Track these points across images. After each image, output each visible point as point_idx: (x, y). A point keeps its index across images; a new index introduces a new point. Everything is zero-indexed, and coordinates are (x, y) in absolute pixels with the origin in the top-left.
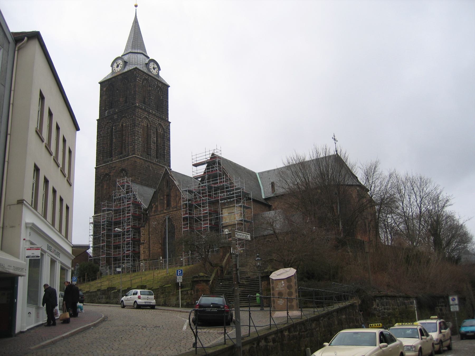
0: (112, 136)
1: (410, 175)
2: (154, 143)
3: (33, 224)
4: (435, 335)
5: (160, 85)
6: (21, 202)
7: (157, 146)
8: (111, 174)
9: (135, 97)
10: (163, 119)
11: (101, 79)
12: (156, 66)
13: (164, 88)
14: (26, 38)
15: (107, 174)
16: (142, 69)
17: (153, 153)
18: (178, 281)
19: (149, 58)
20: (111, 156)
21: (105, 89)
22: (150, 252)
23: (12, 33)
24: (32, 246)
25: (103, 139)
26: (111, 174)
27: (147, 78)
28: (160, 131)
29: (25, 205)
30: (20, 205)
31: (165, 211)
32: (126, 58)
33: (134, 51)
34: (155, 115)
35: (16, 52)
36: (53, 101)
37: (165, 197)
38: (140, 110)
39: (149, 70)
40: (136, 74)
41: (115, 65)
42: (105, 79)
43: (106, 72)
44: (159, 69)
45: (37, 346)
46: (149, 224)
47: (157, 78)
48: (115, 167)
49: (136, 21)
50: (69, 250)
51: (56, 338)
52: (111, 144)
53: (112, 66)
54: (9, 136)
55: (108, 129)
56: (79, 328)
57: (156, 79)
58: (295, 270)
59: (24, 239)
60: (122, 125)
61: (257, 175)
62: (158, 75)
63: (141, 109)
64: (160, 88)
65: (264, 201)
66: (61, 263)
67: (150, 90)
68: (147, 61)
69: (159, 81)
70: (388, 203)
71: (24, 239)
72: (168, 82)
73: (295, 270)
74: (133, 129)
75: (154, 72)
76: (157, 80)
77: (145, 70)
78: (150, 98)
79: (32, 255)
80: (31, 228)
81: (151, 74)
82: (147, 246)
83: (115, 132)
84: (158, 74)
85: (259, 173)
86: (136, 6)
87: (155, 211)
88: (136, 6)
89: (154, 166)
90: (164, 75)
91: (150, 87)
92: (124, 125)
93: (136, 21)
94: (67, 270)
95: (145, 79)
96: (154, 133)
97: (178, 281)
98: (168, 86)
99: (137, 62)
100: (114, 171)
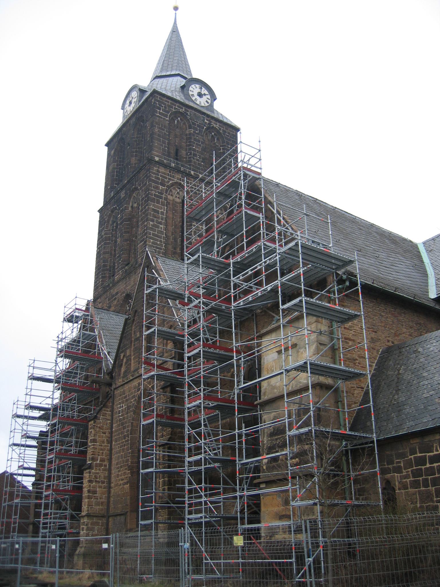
4: (155, 168)
12: (204, 91)
21: (112, 152)
22: (109, 492)
25: (105, 244)
33: (164, 74)
38: (162, 170)
39: (188, 97)
40: (154, 103)
43: (114, 121)
44: (213, 97)
46: (112, 411)
49: (175, 31)
57: (204, 114)
60: (132, 207)
61: (422, 249)
63: (166, 166)
64: (218, 132)
65: (432, 304)
67: (190, 134)
68: (183, 82)
69: (213, 118)
72: (233, 119)
74: (145, 207)
75: (202, 102)
76: (208, 116)
78: (190, 149)
81: (191, 104)
84: (211, 105)
85: (424, 243)
86: (176, 8)
88: (176, 8)
90: (225, 109)
91: (190, 127)
93: (175, 31)
95: (177, 114)
98: (238, 130)
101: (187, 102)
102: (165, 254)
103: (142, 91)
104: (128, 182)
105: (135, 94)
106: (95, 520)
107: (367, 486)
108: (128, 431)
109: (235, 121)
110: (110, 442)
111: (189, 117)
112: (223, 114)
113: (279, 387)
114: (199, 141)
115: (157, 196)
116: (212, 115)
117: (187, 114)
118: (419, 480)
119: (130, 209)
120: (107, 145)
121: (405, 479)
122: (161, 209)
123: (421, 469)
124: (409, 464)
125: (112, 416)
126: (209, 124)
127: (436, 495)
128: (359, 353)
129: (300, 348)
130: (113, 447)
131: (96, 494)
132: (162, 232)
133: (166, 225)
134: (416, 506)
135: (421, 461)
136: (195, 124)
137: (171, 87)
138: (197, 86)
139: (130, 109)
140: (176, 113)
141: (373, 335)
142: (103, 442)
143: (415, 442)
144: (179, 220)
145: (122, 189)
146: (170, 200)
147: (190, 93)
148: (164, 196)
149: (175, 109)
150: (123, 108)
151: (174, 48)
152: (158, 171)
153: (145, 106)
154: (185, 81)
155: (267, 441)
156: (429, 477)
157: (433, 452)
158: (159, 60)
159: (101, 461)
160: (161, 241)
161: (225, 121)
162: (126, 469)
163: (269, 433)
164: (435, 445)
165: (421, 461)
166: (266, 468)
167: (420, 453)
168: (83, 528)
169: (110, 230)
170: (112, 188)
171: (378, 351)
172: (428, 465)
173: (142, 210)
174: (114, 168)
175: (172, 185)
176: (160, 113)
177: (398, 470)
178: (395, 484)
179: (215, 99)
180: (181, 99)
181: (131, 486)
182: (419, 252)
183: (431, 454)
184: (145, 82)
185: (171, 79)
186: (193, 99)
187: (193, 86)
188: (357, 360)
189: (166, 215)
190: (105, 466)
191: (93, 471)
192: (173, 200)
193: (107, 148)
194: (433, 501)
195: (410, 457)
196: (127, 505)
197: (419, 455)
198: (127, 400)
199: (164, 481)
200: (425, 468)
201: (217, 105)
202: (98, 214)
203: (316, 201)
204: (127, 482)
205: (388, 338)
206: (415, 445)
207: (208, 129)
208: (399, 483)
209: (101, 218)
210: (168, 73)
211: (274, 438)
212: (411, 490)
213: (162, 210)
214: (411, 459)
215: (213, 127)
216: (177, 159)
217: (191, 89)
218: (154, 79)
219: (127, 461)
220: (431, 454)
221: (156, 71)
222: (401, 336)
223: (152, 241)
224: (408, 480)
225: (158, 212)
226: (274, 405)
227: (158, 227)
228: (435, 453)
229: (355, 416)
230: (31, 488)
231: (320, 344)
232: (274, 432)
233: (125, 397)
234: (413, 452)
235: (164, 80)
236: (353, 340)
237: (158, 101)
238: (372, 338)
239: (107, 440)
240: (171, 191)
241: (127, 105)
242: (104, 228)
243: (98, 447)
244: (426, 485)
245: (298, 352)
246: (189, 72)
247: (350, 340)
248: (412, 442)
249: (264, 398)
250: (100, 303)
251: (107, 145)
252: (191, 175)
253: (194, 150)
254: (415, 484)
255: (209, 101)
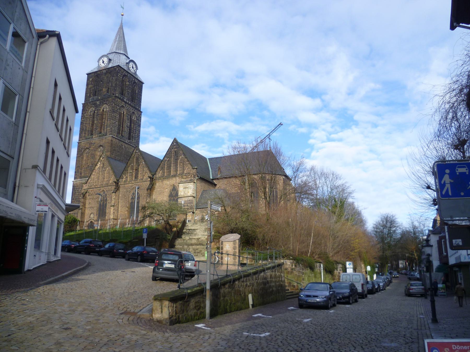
0: (94, 118)
1: (325, 171)
2: (128, 127)
3: (43, 186)
5: (137, 81)
6: (35, 167)
7: (130, 130)
8: (91, 149)
9: (117, 90)
10: (136, 109)
11: (89, 71)
12: (134, 66)
13: (140, 84)
14: (48, 36)
15: (87, 148)
16: (123, 67)
17: (126, 134)
18: (144, 237)
19: (129, 58)
20: (92, 134)
21: (91, 79)
23: (37, 30)
24: (41, 203)
26: (91, 149)
27: (126, 74)
28: (134, 118)
29: (38, 170)
30: (34, 170)
31: (133, 182)
32: (111, 57)
34: (130, 105)
35: (38, 46)
36: (63, 89)
37: (134, 171)
38: (119, 100)
41: (101, 61)
42: (92, 72)
45: (45, 282)
47: (134, 76)
48: (94, 143)
50: (64, 207)
51: (64, 274)
52: (93, 125)
53: (98, 62)
54: (28, 114)
55: (91, 112)
56: (75, 269)
57: (133, 76)
58: (240, 236)
59: (36, 197)
60: (103, 110)
61: (208, 160)
62: (135, 73)
63: (120, 99)
66: (58, 218)
68: (128, 61)
70: (304, 190)
71: (36, 197)
73: (240, 236)
75: (132, 70)
76: (135, 77)
77: (125, 68)
79: (41, 210)
80: (41, 189)
81: (129, 71)
82: (116, 208)
83: (97, 115)
84: (136, 72)
87: (125, 181)
89: (126, 145)
90: (141, 74)
92: (105, 110)
94: (61, 224)
96: (128, 119)
97: (144, 237)
98: (143, 83)
99: (121, 61)
100: (93, 146)
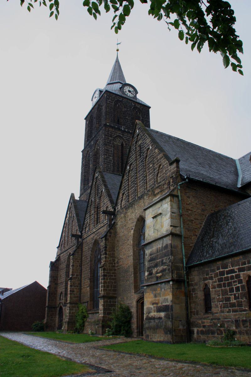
21: (88, 122)
33: (112, 82)
38: (111, 129)
39: (124, 93)
43: (88, 106)
44: (136, 92)
49: (117, 61)
60: (97, 149)
63: (112, 127)
69: (136, 102)
76: (134, 101)
81: (125, 96)
84: (136, 96)
88: (118, 50)
90: (142, 97)
93: (117, 61)
98: (150, 108)
101: (123, 95)
102: (113, 172)
103: (101, 91)
104: (95, 136)
105: (98, 93)
106: (73, 305)
107: (196, 287)
108: (88, 261)
109: (148, 103)
110: (81, 266)
111: (124, 103)
112: (142, 100)
113: (153, 236)
114: (130, 114)
115: (109, 143)
116: (136, 101)
117: (123, 101)
118: (221, 284)
119: (96, 150)
120: (85, 119)
121: (214, 283)
122: (110, 148)
123: (222, 278)
124: (216, 275)
125: (82, 253)
126: (135, 105)
127: (229, 291)
128: (195, 217)
129: (163, 215)
130: (82, 269)
131: (74, 292)
132: (111, 161)
133: (113, 157)
134: (220, 298)
135: (222, 273)
136: (127, 106)
137: (115, 88)
138: (128, 87)
139: (95, 100)
140: (117, 101)
141: (203, 207)
142: (78, 266)
143: (219, 263)
144: (120, 154)
145: (92, 140)
146: (115, 144)
147: (125, 91)
148: (112, 142)
149: (117, 99)
150: (92, 100)
151: (117, 67)
152: (109, 130)
153: (102, 98)
154: (121, 85)
155: (147, 265)
156: (226, 282)
157: (228, 268)
158: (110, 75)
159: (76, 276)
160: (111, 165)
161: (143, 103)
162: (88, 280)
163: (148, 260)
164: (229, 264)
165: (222, 273)
166: (147, 278)
167: (222, 269)
168: (68, 309)
169: (87, 161)
170: (88, 140)
171: (206, 216)
172: (226, 276)
173: (101, 150)
174: (88, 130)
175: (116, 136)
176: (109, 101)
177: (211, 278)
178: (210, 286)
179: (137, 93)
180: (120, 94)
181: (90, 288)
182: (236, 164)
183: (227, 269)
184: (103, 87)
185: (115, 85)
186: (126, 93)
187: (126, 87)
188: (193, 220)
189: (113, 152)
190: (79, 278)
191: (73, 281)
192: (117, 144)
193: (85, 120)
194: (228, 295)
195: (217, 271)
196: (88, 298)
197: (221, 270)
198: (88, 245)
199: (102, 286)
200: (224, 277)
201: (138, 96)
202: (81, 153)
203: (178, 139)
204: (88, 286)
205: (212, 209)
206: (219, 265)
207: (134, 108)
208: (212, 285)
209: (83, 155)
210: (114, 82)
211: (151, 263)
212: (217, 289)
213: (111, 150)
214: (217, 272)
215: (137, 107)
216: (119, 124)
217: (125, 88)
218: (107, 85)
219: (88, 275)
220: (227, 269)
221: (108, 81)
222: (219, 207)
223: (106, 165)
224: (216, 284)
225: (109, 151)
226: (151, 245)
227: (109, 158)
228: (229, 269)
229: (192, 251)
230: (47, 289)
231: (172, 213)
232: (150, 259)
233: (87, 244)
234: (218, 269)
235: (112, 85)
236: (192, 211)
237: (108, 95)
238: (202, 209)
239: (79, 265)
240: (115, 140)
241: (94, 99)
242: (84, 160)
243: (75, 269)
244: (225, 286)
245: (162, 217)
246: (124, 80)
247: (190, 210)
248: (218, 263)
249: (146, 242)
250: (83, 197)
251: (85, 119)
252: (126, 131)
253: (127, 119)
254: (220, 286)
255: (134, 94)
